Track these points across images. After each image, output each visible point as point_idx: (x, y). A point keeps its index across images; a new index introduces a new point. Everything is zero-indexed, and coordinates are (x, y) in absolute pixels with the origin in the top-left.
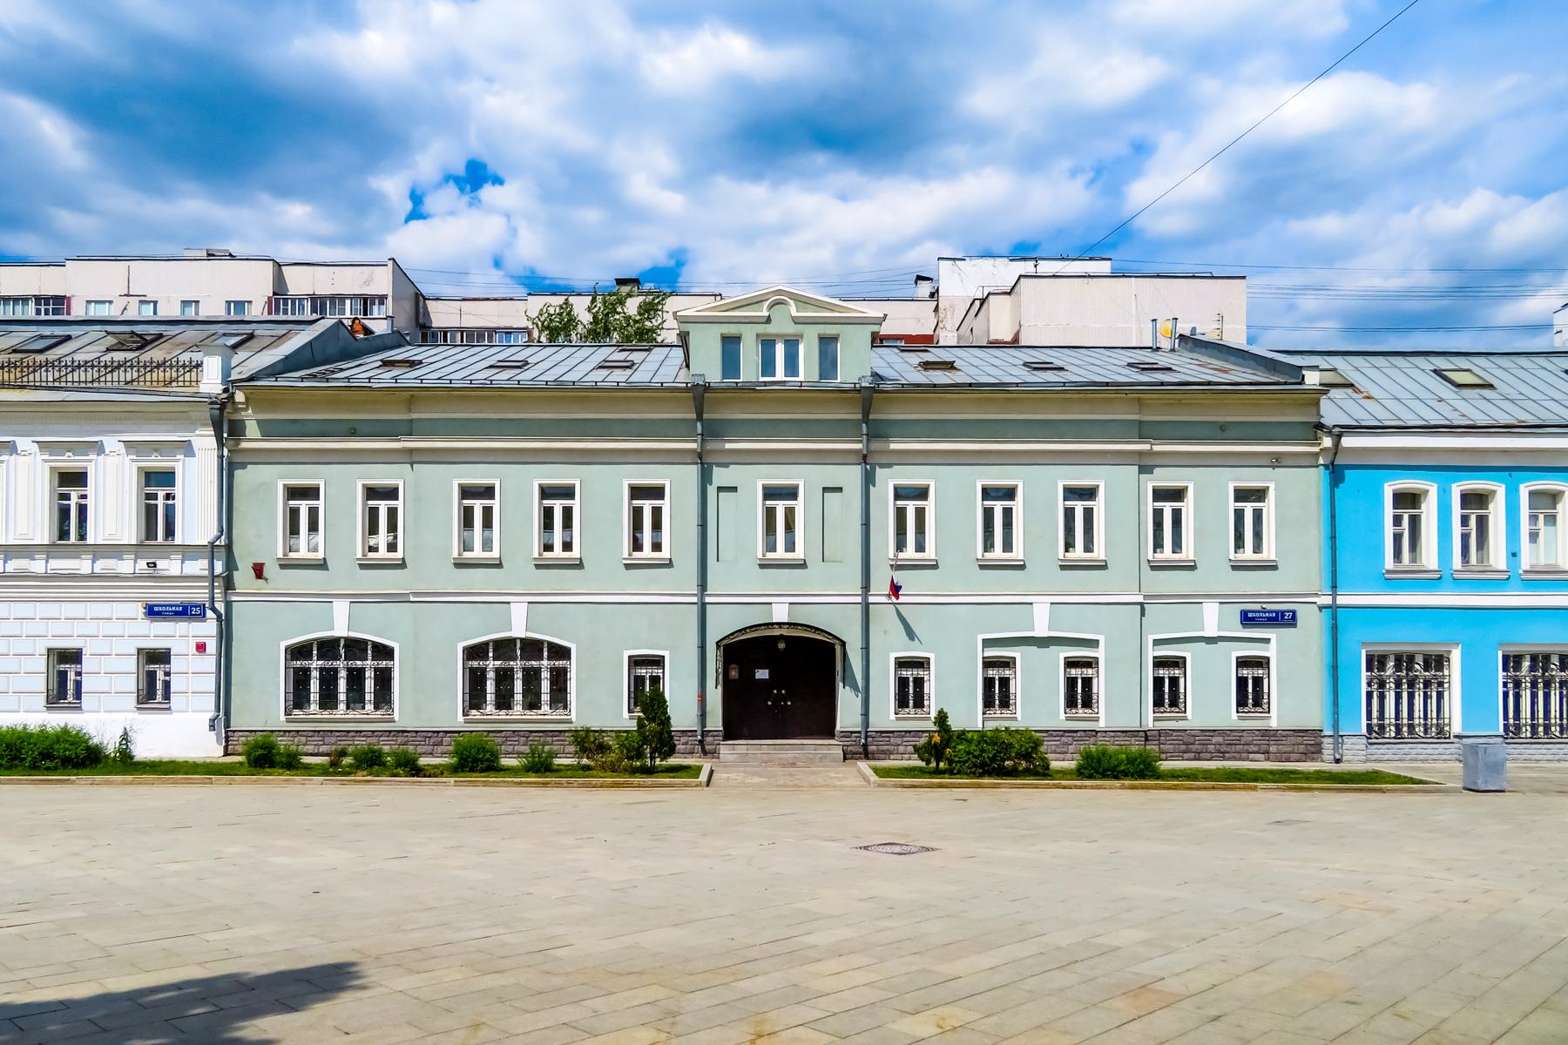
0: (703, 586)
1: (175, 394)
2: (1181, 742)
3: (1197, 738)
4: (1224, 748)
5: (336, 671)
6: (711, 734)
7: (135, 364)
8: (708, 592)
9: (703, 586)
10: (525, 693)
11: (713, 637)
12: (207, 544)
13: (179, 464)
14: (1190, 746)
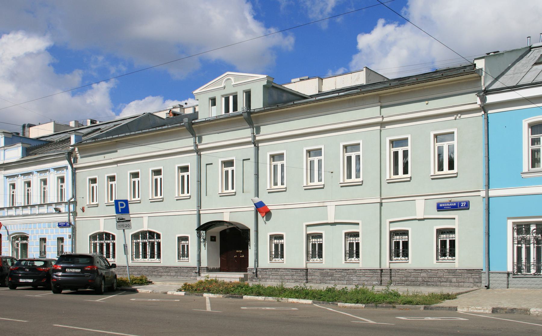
2: (404, 276)
3: (412, 274)
4: (427, 279)
6: (203, 268)
8: (202, 209)
12: (67, 201)
14: (408, 278)
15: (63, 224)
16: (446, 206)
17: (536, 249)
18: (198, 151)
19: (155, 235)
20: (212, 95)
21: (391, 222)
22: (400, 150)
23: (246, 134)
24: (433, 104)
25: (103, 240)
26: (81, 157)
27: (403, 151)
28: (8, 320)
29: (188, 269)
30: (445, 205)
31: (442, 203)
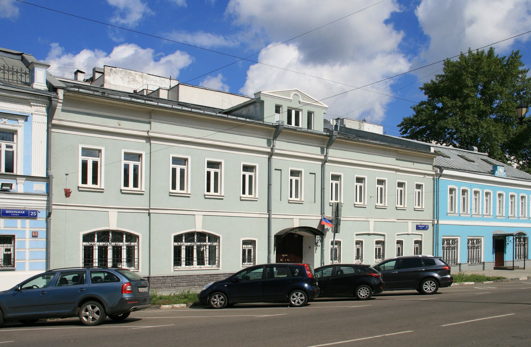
0: (269, 210)
1: (17, 87)
5: (193, 247)
7: (24, 74)
9: (269, 210)
10: (198, 259)
11: (274, 233)
13: (20, 126)
15: (422, 227)
16: (14, 214)
17: (11, 257)
18: (271, 155)
19: (125, 236)
20: (279, 103)
21: (397, 235)
22: (90, 161)
23: (315, 151)
24: (417, 165)
25: (108, 241)
26: (63, 110)
27: (214, 172)
28: (400, 332)
29: (256, 274)
30: (12, 212)
31: (9, 210)
